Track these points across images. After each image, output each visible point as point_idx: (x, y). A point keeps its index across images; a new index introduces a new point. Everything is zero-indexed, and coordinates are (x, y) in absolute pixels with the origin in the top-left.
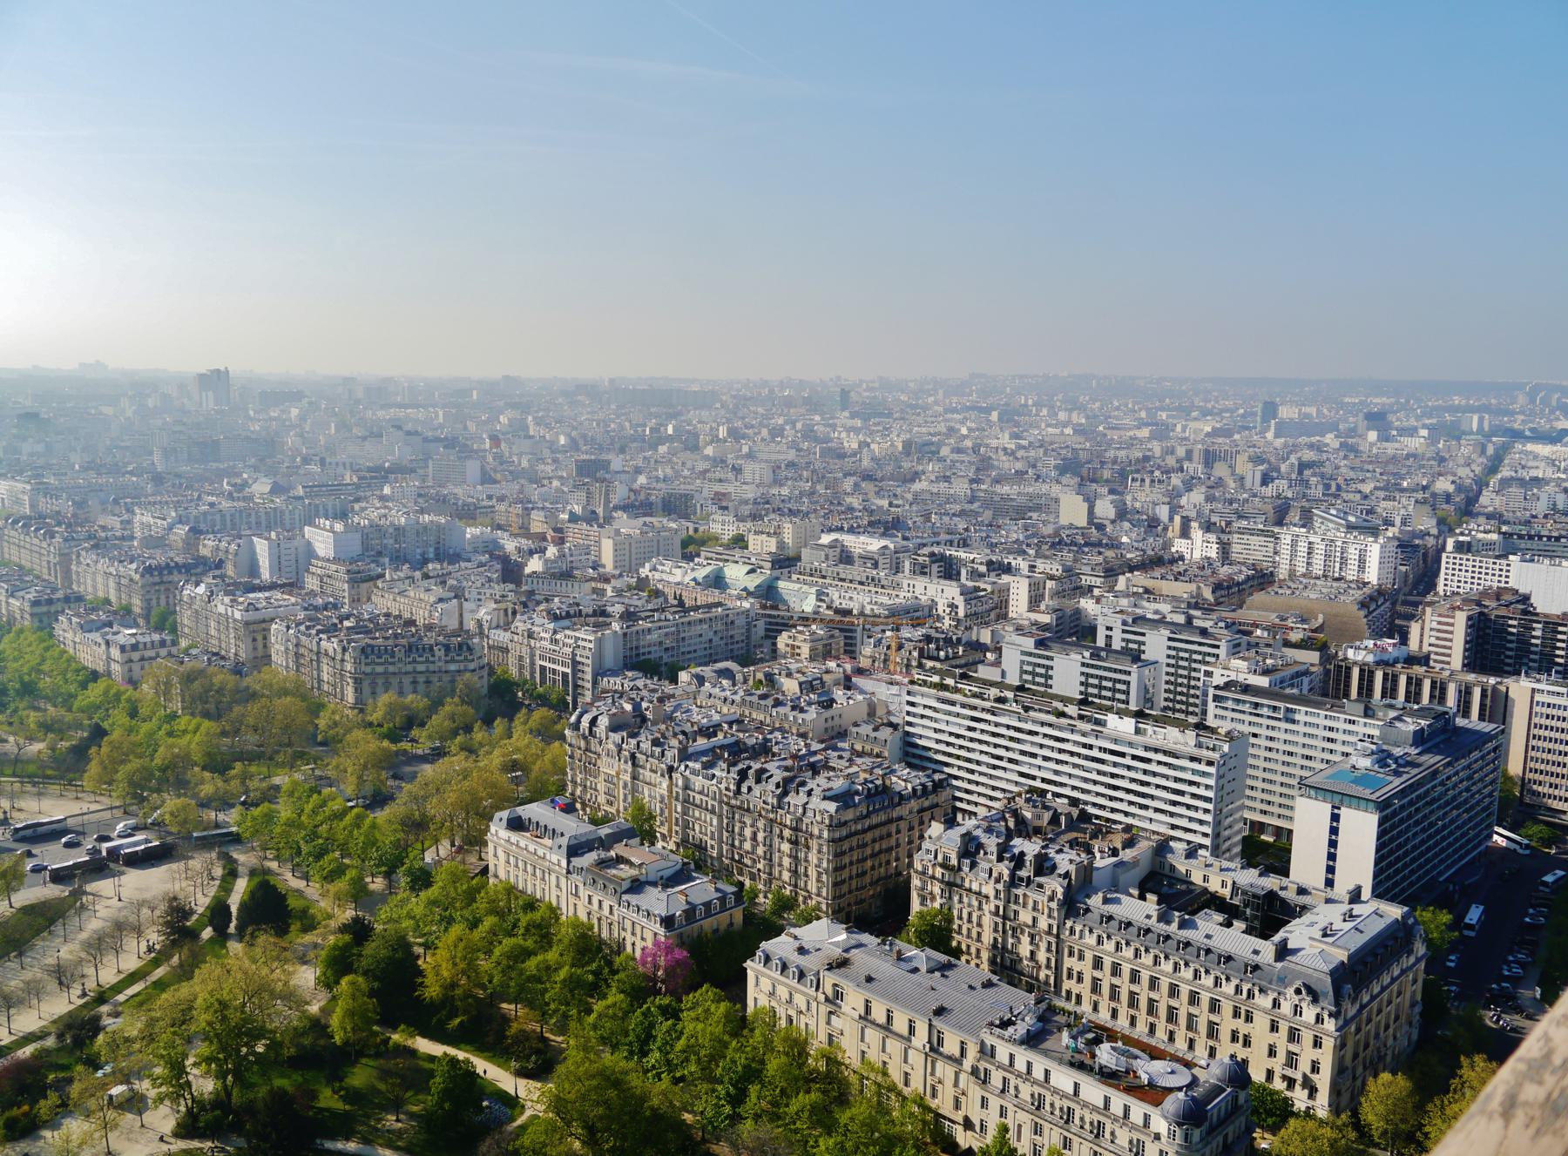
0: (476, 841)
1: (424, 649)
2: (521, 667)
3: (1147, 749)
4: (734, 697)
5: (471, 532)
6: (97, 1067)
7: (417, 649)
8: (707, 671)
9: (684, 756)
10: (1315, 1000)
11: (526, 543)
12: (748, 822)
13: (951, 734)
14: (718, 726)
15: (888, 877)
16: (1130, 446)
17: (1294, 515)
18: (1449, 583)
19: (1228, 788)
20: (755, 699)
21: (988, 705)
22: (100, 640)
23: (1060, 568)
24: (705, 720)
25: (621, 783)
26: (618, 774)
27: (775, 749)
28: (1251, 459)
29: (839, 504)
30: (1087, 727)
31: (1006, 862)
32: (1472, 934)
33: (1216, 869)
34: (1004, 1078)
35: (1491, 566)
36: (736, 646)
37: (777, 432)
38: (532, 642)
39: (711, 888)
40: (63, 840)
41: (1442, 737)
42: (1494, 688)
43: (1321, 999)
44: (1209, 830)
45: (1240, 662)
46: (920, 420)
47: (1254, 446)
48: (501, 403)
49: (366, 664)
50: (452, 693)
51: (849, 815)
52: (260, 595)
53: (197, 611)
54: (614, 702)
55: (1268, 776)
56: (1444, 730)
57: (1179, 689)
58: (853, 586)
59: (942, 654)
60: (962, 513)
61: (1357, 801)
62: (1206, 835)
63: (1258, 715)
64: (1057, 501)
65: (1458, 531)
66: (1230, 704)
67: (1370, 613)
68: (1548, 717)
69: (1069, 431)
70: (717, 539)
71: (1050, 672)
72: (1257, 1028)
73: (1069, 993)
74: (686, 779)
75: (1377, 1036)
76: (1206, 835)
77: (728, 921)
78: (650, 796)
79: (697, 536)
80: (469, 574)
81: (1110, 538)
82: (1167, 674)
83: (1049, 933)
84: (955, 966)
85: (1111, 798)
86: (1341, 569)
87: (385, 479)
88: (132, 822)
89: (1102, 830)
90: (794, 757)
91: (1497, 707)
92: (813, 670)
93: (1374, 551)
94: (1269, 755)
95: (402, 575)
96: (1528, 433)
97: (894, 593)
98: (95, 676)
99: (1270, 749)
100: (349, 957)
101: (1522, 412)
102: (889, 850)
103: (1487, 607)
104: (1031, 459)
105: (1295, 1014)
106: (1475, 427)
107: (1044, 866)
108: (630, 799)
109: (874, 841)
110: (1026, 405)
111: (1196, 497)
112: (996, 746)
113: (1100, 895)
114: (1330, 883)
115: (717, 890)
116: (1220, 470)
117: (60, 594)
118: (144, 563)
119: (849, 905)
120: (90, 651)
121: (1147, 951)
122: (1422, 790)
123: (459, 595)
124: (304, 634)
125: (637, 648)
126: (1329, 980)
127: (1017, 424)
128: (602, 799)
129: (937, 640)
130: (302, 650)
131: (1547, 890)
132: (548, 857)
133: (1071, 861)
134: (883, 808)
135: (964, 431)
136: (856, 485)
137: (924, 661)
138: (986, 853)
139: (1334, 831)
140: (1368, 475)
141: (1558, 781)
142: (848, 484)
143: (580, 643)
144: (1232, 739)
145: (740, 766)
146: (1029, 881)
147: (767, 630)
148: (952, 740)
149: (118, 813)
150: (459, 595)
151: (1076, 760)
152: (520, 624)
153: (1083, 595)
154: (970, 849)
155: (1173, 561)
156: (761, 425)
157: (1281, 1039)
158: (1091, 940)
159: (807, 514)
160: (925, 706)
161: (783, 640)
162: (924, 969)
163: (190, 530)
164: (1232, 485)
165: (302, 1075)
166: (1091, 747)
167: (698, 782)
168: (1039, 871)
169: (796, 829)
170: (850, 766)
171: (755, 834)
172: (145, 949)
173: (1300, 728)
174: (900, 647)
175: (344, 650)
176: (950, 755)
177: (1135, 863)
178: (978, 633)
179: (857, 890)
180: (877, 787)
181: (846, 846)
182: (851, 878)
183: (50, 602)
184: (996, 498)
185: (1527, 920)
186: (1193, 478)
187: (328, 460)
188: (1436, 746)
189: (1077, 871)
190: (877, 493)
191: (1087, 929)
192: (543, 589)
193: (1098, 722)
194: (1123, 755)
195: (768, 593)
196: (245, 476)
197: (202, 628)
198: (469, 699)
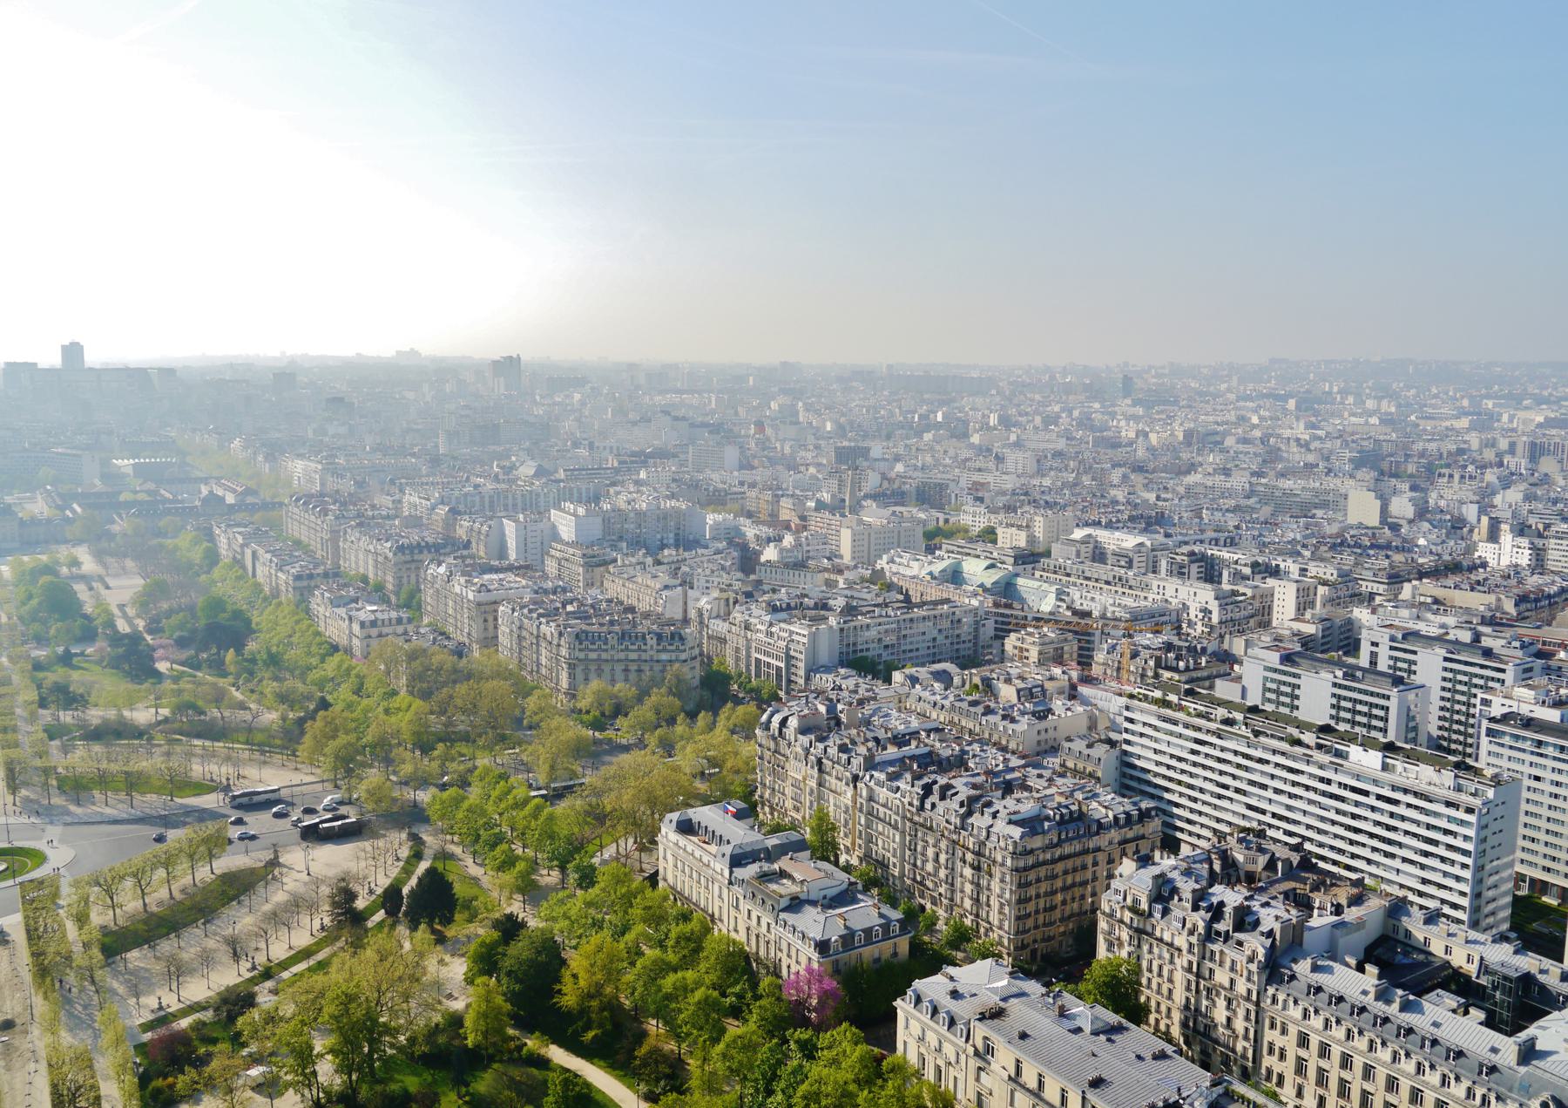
0: (648, 843)
1: (636, 637)
2: (738, 659)
3: (1394, 788)
4: (944, 702)
5: (711, 518)
6: (244, 1045)
8: (923, 672)
9: (870, 764)
11: (766, 531)
12: (931, 841)
13: (1172, 756)
14: (915, 734)
15: (1082, 913)
19: (1492, 840)
20: (965, 705)
21: (1213, 726)
22: (344, 616)
23: (1335, 573)
24: (903, 727)
26: (805, 779)
27: (971, 764)
29: (1102, 496)
30: (1326, 758)
31: (1202, 912)
33: (1461, 939)
36: (961, 646)
38: (749, 633)
39: (875, 912)
40: (274, 810)
46: (1209, 408)
48: (775, 389)
50: (659, 685)
51: (1037, 842)
52: (495, 576)
54: (807, 702)
57: (1456, 717)
59: (1182, 664)
60: (1236, 509)
62: (1463, 894)
63: (1541, 755)
64: (1346, 497)
66: (1507, 740)
69: (1374, 420)
70: (967, 531)
71: (1297, 692)
73: (1269, 1072)
76: (1463, 894)
77: (891, 951)
78: (835, 805)
79: (946, 528)
80: (701, 564)
81: (1405, 540)
83: (1248, 999)
85: (1352, 842)
87: (644, 464)
88: (337, 796)
89: (1326, 881)
90: (989, 773)
92: (1036, 675)
94: (1554, 802)
95: (633, 560)
97: (1143, 595)
98: (335, 648)
99: (1556, 796)
100: (495, 955)
102: (1084, 883)
104: (1325, 451)
107: (1245, 920)
108: (815, 807)
109: (1066, 872)
110: (1330, 393)
111: (1514, 495)
112: (1221, 773)
113: (1309, 961)
115: (881, 915)
117: (320, 570)
118: (397, 541)
119: (1035, 941)
120: (335, 624)
121: (1361, 1033)
123: (687, 583)
124: (527, 618)
125: (854, 644)
127: (1316, 414)
128: (789, 804)
129: (1180, 648)
130: (524, 633)
133: (1277, 918)
134: (1078, 837)
135: (1255, 420)
136: (1125, 477)
137: (1161, 671)
142: (1116, 476)
143: (795, 637)
144: (1498, 783)
145: (926, 780)
147: (996, 629)
148: (1173, 763)
149: (329, 786)
151: (1311, 795)
152: (738, 615)
154: (1163, 893)
155: (1473, 568)
158: (1296, 1013)
159: (1064, 508)
160: (1145, 724)
161: (1011, 642)
162: (1088, 1029)
165: (433, 1075)
166: (1329, 782)
167: (883, 794)
168: (1240, 926)
170: (1049, 787)
172: (319, 927)
174: (1134, 655)
175: (561, 634)
176: (1170, 779)
177: (1360, 924)
178: (1231, 643)
179: (1045, 925)
180: (1071, 812)
181: (1032, 876)
182: (1037, 912)
183: (311, 576)
186: (1512, 474)
190: (1146, 486)
192: (769, 579)
193: (1339, 754)
194: (1366, 793)
195: (1006, 591)
197: (442, 607)
198: (678, 690)
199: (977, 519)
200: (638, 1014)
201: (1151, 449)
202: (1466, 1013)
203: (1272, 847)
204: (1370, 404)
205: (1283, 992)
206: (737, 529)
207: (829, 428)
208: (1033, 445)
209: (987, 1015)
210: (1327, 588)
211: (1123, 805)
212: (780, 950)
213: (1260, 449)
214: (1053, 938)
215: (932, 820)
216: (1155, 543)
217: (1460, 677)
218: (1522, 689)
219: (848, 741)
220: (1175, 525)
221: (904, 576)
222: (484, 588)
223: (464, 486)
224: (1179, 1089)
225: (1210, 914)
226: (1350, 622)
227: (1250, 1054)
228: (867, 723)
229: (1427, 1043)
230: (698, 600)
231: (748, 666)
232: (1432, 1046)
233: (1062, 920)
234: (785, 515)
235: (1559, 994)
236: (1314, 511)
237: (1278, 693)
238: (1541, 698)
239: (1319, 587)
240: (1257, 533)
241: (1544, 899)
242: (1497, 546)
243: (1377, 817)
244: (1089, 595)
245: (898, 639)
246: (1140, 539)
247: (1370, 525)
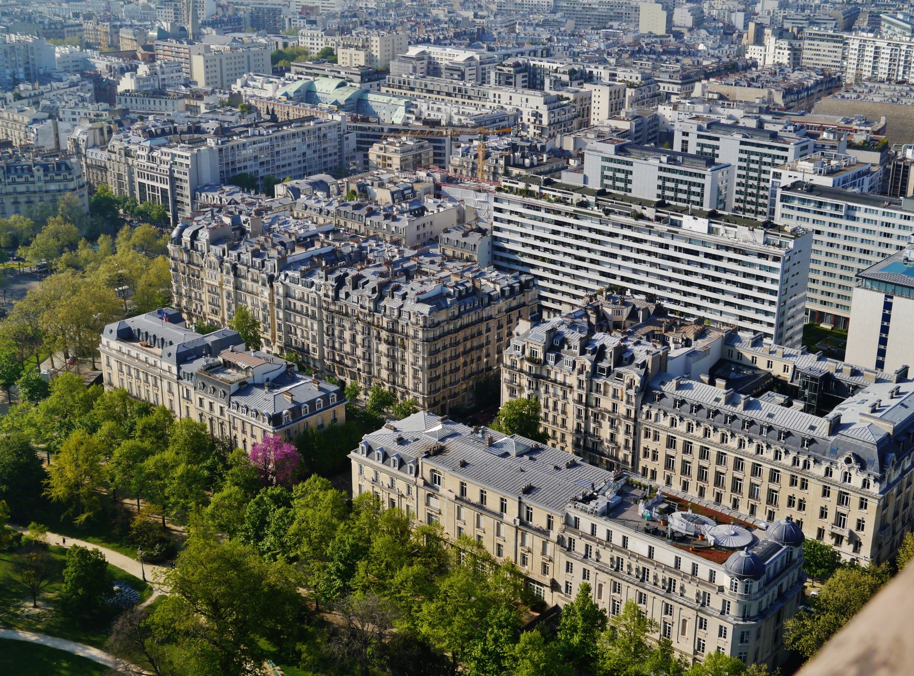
1: (22, 170)
2: (121, 185)
3: (719, 247)
4: (329, 208)
5: (60, 51)
7: (16, 170)
8: (302, 184)
9: (284, 266)
10: (863, 465)
11: (116, 62)
12: (347, 325)
13: (536, 238)
14: (315, 236)
17: (863, 21)
19: (792, 281)
20: (349, 209)
21: (570, 209)
23: (639, 76)
24: (302, 231)
25: (225, 294)
26: (221, 284)
27: (370, 256)
29: (425, 16)
30: (664, 228)
31: (589, 355)
34: (587, 546)
36: (329, 159)
38: (130, 160)
39: (315, 387)
43: (868, 466)
44: (773, 320)
45: (806, 163)
51: (442, 316)
55: (829, 269)
57: (749, 190)
58: (441, 97)
59: (527, 161)
60: (545, 24)
62: (770, 325)
63: (821, 213)
64: (637, 9)
66: (796, 204)
70: (306, 53)
71: (630, 177)
72: (811, 493)
74: (286, 287)
76: (770, 325)
78: (253, 304)
79: (287, 51)
81: (687, 46)
82: (739, 176)
85: (685, 294)
86: (904, 72)
90: (389, 263)
92: (405, 180)
94: (830, 250)
97: (481, 103)
99: (832, 245)
102: (480, 347)
105: (845, 480)
107: (623, 357)
109: (466, 339)
112: (579, 248)
113: (674, 381)
114: (880, 365)
115: (320, 389)
119: (444, 398)
123: (53, 114)
125: (233, 163)
128: (207, 309)
129: (523, 148)
132: (159, 364)
133: (648, 352)
134: (474, 309)
137: (510, 169)
138: (569, 348)
139: (886, 318)
143: (177, 160)
144: (797, 236)
145: (338, 273)
146: (609, 372)
147: (358, 142)
148: (538, 243)
150: (53, 114)
151: (653, 259)
152: (116, 143)
153: (661, 102)
157: (831, 503)
158: (665, 422)
160: (512, 212)
161: (374, 152)
162: (513, 453)
166: (667, 247)
167: (298, 290)
168: (619, 362)
169: (392, 331)
170: (442, 270)
173: (860, 225)
174: (487, 156)
176: (535, 257)
177: (706, 352)
179: (451, 384)
180: (467, 289)
181: (440, 345)
182: (445, 374)
191: (662, 412)
192: (137, 107)
193: (674, 223)
194: (696, 253)
198: (71, 217)
199: (315, 42)
200: (119, 494)
205: (655, 408)
206: (85, 61)
209: (431, 452)
210: (633, 90)
211: (505, 280)
212: (234, 428)
214: (458, 394)
215: (347, 307)
216: (484, 56)
217: (753, 157)
218: (804, 163)
219: (259, 247)
220: (495, 40)
221: (261, 98)
224: (593, 485)
225: (594, 356)
226: (656, 118)
227: (630, 460)
228: (269, 230)
229: (765, 430)
232: (768, 432)
233: (463, 379)
235: (850, 386)
236: (610, 23)
237: (614, 179)
238: (819, 169)
239: (628, 89)
240: (567, 44)
241: (822, 325)
242: (763, 48)
243: (705, 271)
244: (436, 106)
247: (658, 34)
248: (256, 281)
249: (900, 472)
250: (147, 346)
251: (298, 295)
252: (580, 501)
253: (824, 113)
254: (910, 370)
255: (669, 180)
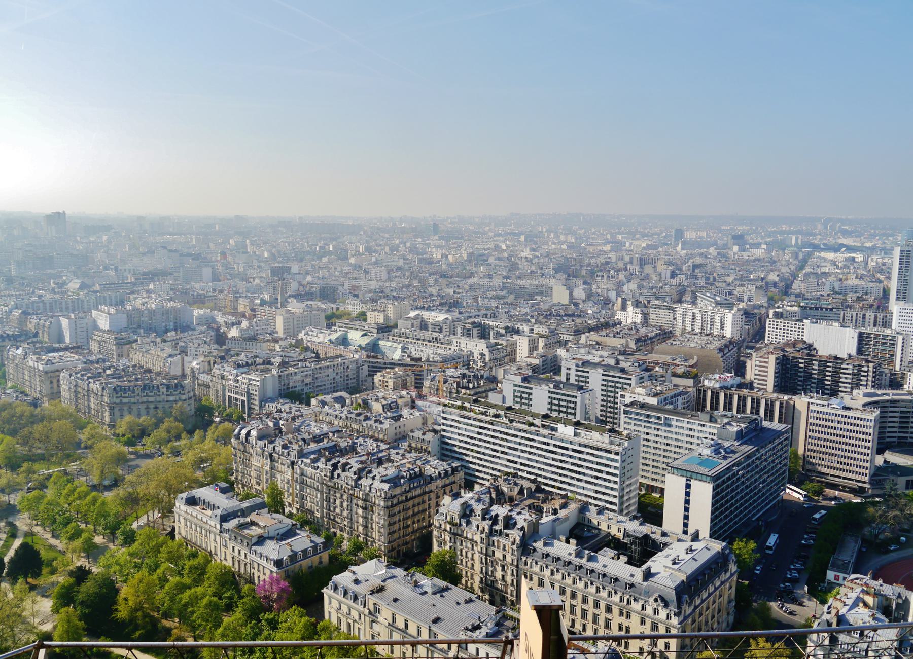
1: (153, 387)
2: (217, 397)
3: (580, 445)
4: (341, 415)
5: (196, 312)
7: (149, 388)
8: (328, 398)
9: (301, 455)
10: (666, 605)
11: (231, 319)
13: (468, 437)
16: (599, 255)
17: (687, 297)
18: (771, 336)
21: (489, 419)
23: (548, 330)
25: (265, 472)
26: (262, 466)
27: (359, 450)
28: (666, 263)
29: (424, 292)
30: (546, 432)
32: (771, 552)
33: (614, 521)
35: (794, 326)
36: (350, 381)
37: (394, 249)
38: (224, 381)
41: (754, 434)
42: (787, 402)
44: (616, 494)
45: (641, 389)
47: (669, 255)
49: (117, 398)
51: (398, 491)
52: (56, 354)
53: (17, 365)
55: (656, 458)
56: (755, 430)
57: (609, 404)
59: (471, 386)
60: (496, 297)
61: (700, 477)
62: (615, 497)
63: (649, 422)
64: (552, 289)
65: (776, 305)
67: (724, 355)
68: (817, 419)
69: (564, 247)
70: (349, 314)
71: (531, 397)
75: (706, 623)
76: (615, 497)
78: (281, 479)
79: (338, 313)
80: (190, 340)
83: (512, 564)
84: (450, 589)
85: (561, 475)
87: (152, 280)
89: (548, 497)
91: (789, 414)
92: (392, 396)
93: (729, 318)
95: (148, 340)
96: (822, 246)
97: (448, 347)
99: (657, 442)
101: (820, 234)
102: (424, 511)
103: (787, 352)
104: (540, 264)
105: (655, 614)
106: (793, 243)
107: (509, 523)
109: (414, 506)
110: (541, 232)
112: (494, 444)
115: (312, 541)
116: (648, 269)
119: (399, 546)
122: (730, 474)
123: (183, 352)
124: (80, 379)
126: (674, 593)
128: (253, 481)
129: (469, 376)
130: (79, 389)
131: (816, 523)
132: (209, 522)
133: (525, 520)
134: (420, 486)
135: (504, 247)
136: (436, 280)
137: (460, 390)
138: (476, 515)
139: (688, 494)
140: (732, 271)
141: (824, 456)
142: (431, 280)
143: (252, 382)
144: (630, 438)
145: (333, 461)
146: (500, 533)
147: (369, 371)
148: (469, 440)
152: (216, 371)
155: (615, 325)
156: (386, 244)
158: (536, 569)
160: (453, 420)
161: (378, 377)
162: (430, 591)
163: (22, 313)
164: (655, 278)
166: (548, 444)
167: (309, 471)
168: (507, 526)
169: (365, 500)
170: (403, 459)
171: (342, 503)
173: (673, 429)
174: (445, 382)
175: (103, 389)
176: (467, 449)
177: (567, 518)
178: (496, 371)
180: (415, 473)
181: (396, 510)
184: (517, 288)
185: (803, 542)
187: (120, 268)
188: (750, 439)
189: (528, 526)
190: (448, 285)
192: (235, 348)
193: (553, 429)
194: (567, 449)
195: (373, 348)
196: (64, 278)
197: (20, 375)
198: (181, 418)
199: (355, 307)
201: (449, 265)
202: (619, 558)
203: (521, 482)
204: (562, 238)
207: (266, 255)
208: (385, 264)
212: (253, 568)
213: (507, 263)
216: (454, 318)
217: (610, 384)
221: (315, 342)
222: (49, 362)
223: (31, 297)
228: (298, 430)
230: (191, 362)
231: (224, 401)
234: (241, 309)
244: (420, 349)
245: (313, 379)
246: (445, 316)
248: (284, 465)
249: (693, 607)
250: (203, 509)
251: (309, 474)
252: (470, 630)
253: (661, 353)
254: (700, 532)
255: (555, 399)
